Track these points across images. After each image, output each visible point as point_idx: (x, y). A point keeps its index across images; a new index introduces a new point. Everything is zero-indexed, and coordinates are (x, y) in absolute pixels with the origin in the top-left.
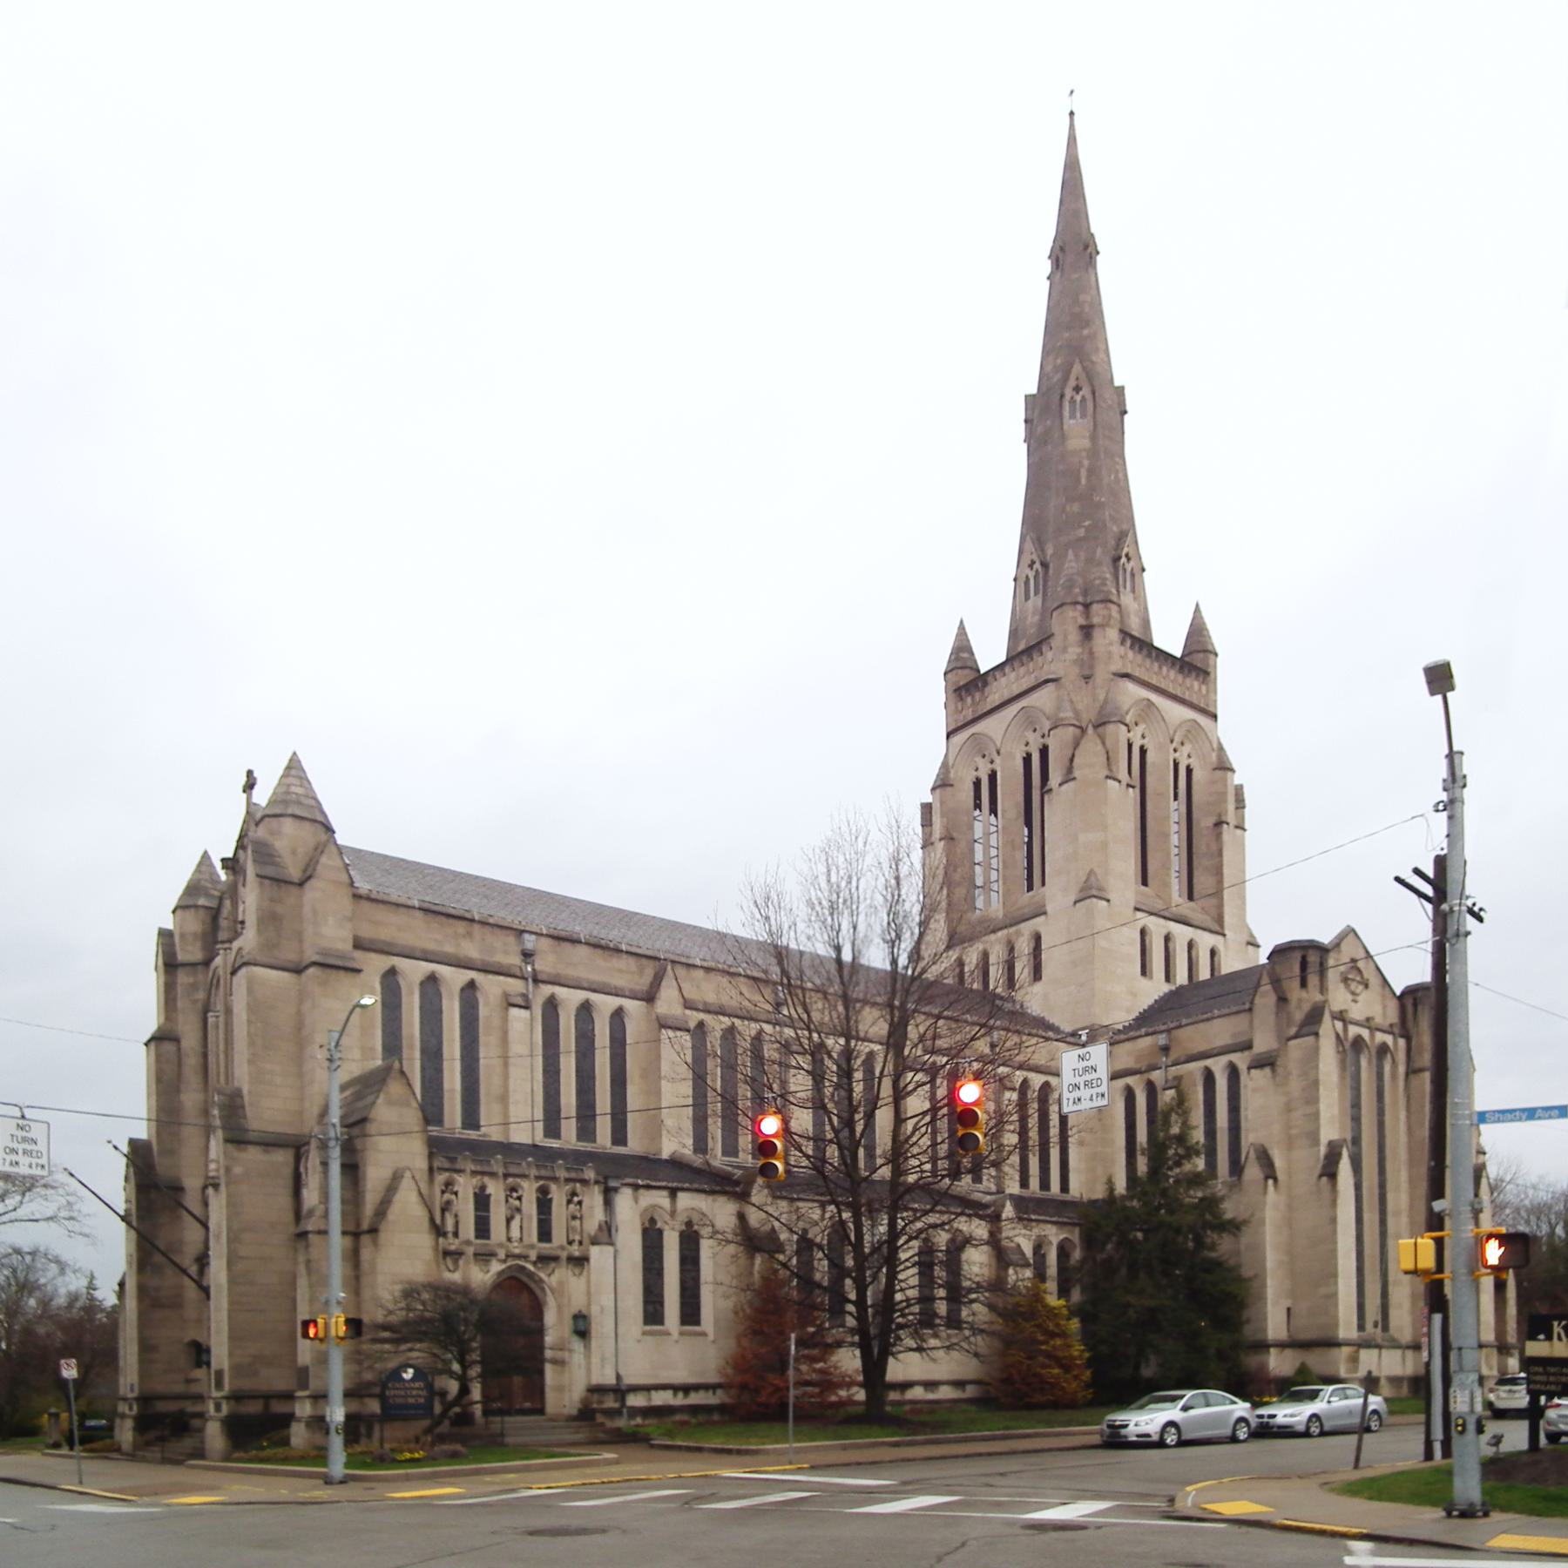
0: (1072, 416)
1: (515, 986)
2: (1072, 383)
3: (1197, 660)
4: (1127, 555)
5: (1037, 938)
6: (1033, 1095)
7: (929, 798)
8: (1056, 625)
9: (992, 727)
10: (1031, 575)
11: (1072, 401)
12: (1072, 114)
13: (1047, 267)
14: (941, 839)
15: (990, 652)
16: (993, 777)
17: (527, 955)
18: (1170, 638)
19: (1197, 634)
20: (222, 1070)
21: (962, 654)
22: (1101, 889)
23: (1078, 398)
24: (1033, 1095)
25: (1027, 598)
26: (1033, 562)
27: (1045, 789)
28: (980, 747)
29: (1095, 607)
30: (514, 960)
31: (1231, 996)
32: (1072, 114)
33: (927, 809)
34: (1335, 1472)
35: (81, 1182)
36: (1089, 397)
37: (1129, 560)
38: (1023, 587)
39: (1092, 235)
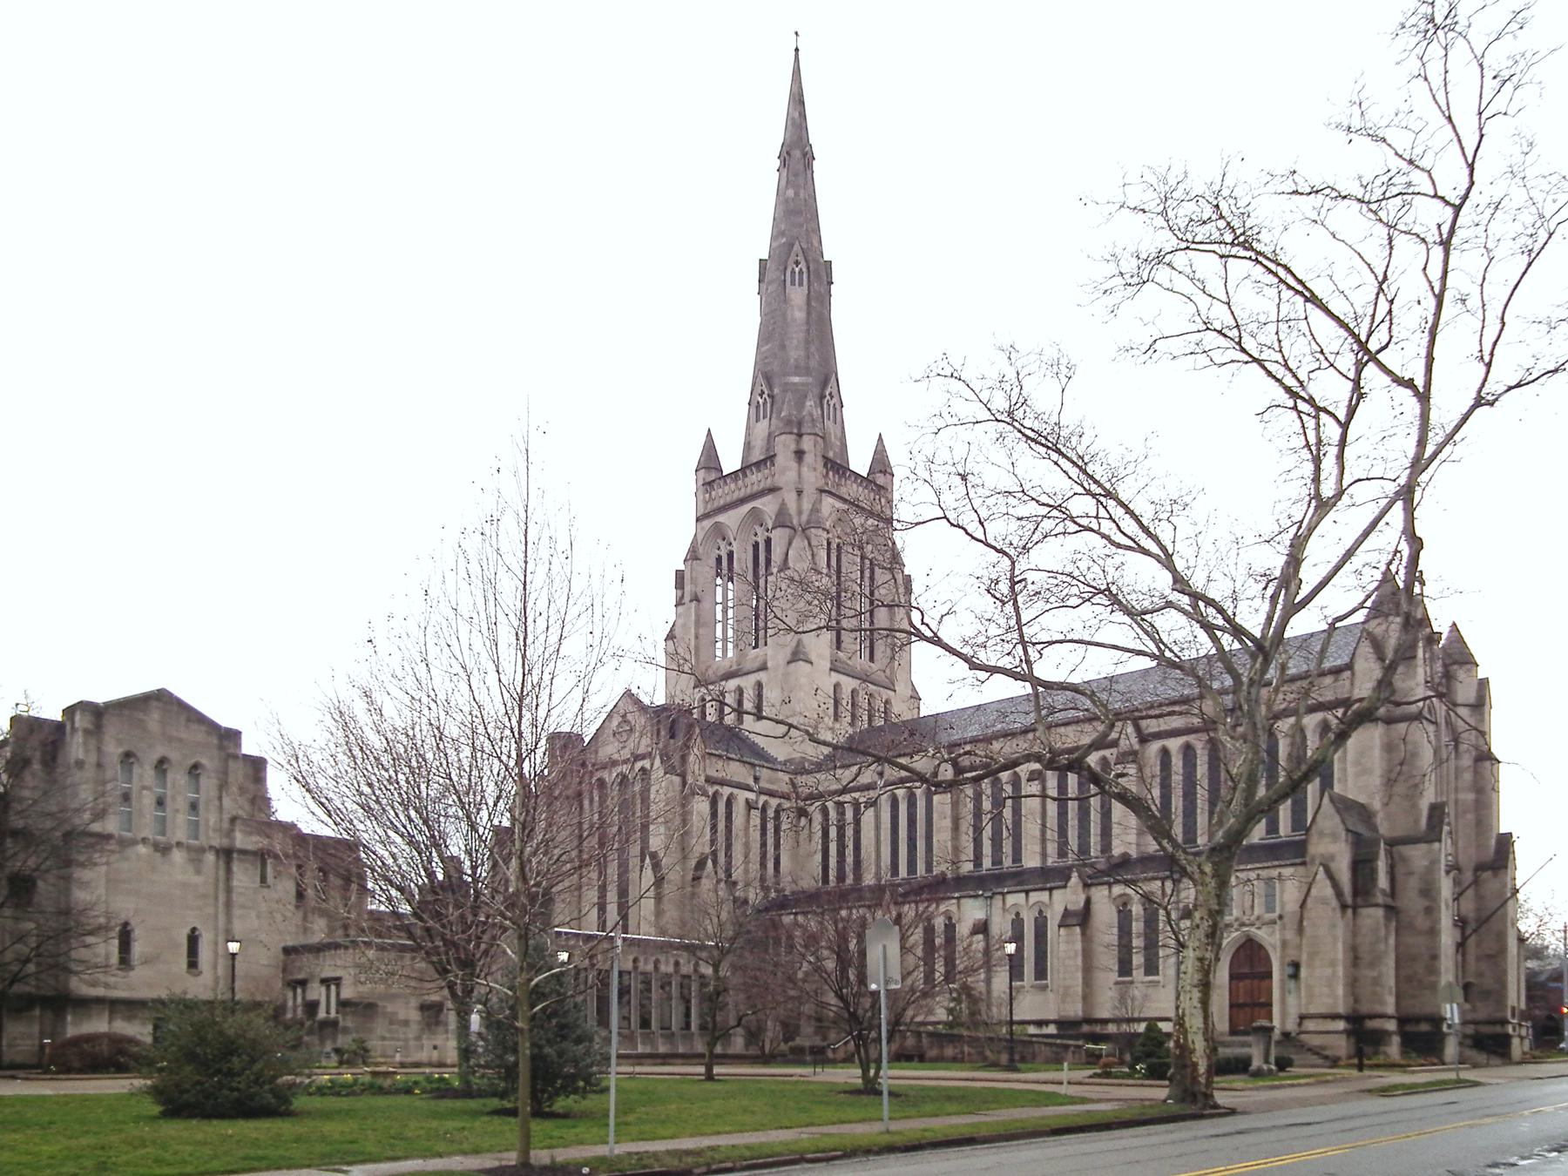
0: (793, 283)
1: (752, 796)
2: (792, 258)
3: (880, 479)
4: (830, 394)
5: (759, 685)
6: (771, 813)
7: (682, 567)
8: (779, 449)
9: (731, 519)
10: (761, 401)
11: (793, 272)
12: (797, 50)
13: (777, 163)
14: (691, 601)
15: (731, 461)
16: (730, 555)
17: (756, 779)
18: (860, 462)
19: (881, 463)
20: (1295, 1082)
21: (709, 459)
22: (805, 654)
23: (797, 270)
24: (771, 813)
25: (757, 420)
26: (763, 392)
27: (768, 573)
28: (719, 532)
29: (805, 438)
30: (751, 782)
31: (530, 568)
32: (797, 50)
33: (680, 576)
34: (115, 988)
35: (1309, 1124)
36: (804, 270)
37: (832, 397)
38: (757, 410)
39: (1485, 757)
